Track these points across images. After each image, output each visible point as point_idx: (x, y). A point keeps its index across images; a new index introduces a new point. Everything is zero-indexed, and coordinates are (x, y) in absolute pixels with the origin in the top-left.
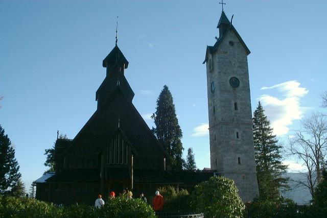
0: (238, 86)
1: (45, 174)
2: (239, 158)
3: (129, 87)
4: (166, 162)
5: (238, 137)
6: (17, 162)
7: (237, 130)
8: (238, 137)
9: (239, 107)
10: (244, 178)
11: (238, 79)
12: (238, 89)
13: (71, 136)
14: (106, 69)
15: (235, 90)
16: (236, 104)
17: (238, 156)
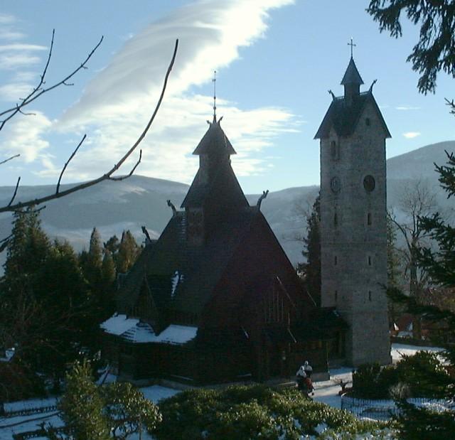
0: (374, 188)
1: (314, 206)
2: (370, 292)
3: (147, 178)
4: (177, 287)
5: (370, 263)
6: (371, 14)
7: (369, 254)
8: (370, 263)
9: (373, 219)
10: (374, 319)
11: (373, 179)
12: (373, 193)
13: (232, 157)
14: (265, 27)
15: (370, 194)
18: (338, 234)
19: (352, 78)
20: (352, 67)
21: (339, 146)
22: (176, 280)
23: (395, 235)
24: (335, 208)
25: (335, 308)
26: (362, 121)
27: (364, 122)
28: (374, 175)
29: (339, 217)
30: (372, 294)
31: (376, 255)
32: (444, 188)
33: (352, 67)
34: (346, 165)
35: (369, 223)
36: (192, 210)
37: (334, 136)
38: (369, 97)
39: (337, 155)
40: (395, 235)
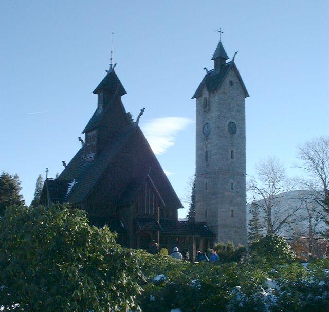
5: (232, 189)
7: (232, 181)
8: (232, 189)
12: (235, 136)
16: (232, 152)
17: (232, 208)
18: (208, 165)
19: (220, 56)
20: (220, 49)
21: (209, 101)
22: (72, 184)
23: (19, 184)
24: (206, 147)
25: (205, 223)
26: (227, 81)
27: (228, 83)
28: (236, 123)
29: (209, 153)
30: (234, 213)
31: (238, 183)
32: (256, 166)
33: (220, 49)
34: (214, 113)
35: (232, 157)
36: (89, 134)
37: (206, 94)
38: (232, 66)
39: (208, 107)
40: (19, 184)
